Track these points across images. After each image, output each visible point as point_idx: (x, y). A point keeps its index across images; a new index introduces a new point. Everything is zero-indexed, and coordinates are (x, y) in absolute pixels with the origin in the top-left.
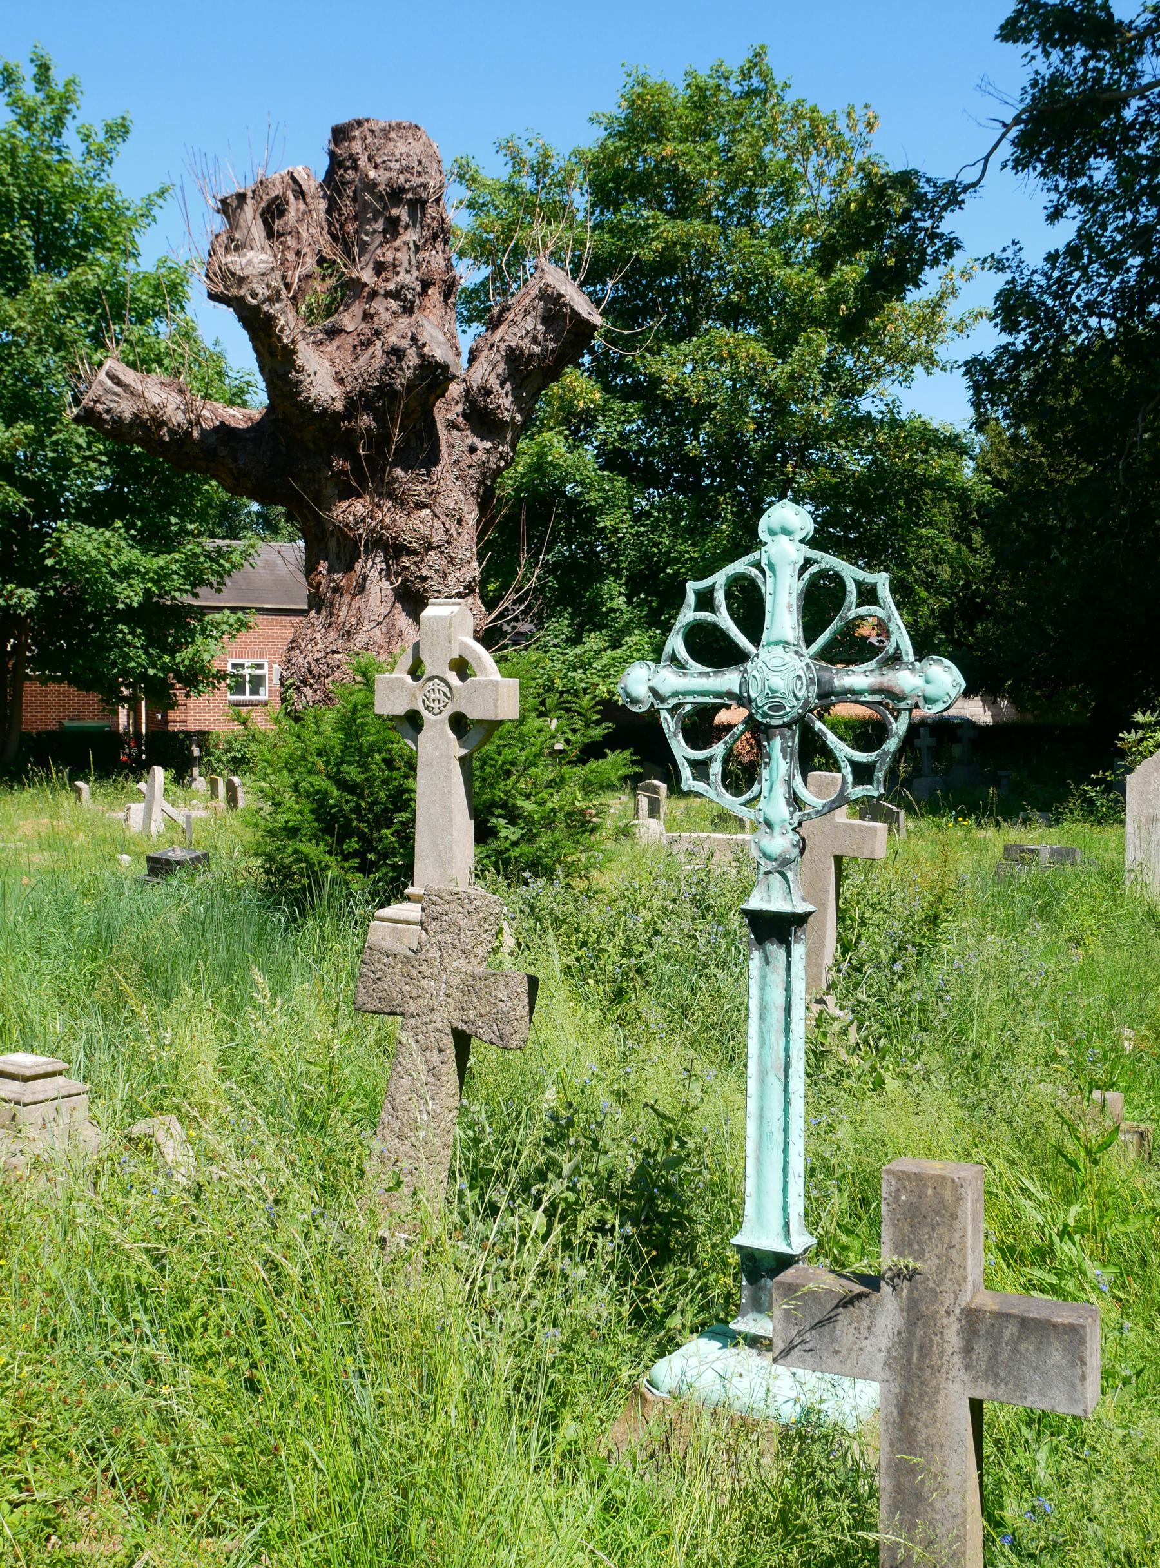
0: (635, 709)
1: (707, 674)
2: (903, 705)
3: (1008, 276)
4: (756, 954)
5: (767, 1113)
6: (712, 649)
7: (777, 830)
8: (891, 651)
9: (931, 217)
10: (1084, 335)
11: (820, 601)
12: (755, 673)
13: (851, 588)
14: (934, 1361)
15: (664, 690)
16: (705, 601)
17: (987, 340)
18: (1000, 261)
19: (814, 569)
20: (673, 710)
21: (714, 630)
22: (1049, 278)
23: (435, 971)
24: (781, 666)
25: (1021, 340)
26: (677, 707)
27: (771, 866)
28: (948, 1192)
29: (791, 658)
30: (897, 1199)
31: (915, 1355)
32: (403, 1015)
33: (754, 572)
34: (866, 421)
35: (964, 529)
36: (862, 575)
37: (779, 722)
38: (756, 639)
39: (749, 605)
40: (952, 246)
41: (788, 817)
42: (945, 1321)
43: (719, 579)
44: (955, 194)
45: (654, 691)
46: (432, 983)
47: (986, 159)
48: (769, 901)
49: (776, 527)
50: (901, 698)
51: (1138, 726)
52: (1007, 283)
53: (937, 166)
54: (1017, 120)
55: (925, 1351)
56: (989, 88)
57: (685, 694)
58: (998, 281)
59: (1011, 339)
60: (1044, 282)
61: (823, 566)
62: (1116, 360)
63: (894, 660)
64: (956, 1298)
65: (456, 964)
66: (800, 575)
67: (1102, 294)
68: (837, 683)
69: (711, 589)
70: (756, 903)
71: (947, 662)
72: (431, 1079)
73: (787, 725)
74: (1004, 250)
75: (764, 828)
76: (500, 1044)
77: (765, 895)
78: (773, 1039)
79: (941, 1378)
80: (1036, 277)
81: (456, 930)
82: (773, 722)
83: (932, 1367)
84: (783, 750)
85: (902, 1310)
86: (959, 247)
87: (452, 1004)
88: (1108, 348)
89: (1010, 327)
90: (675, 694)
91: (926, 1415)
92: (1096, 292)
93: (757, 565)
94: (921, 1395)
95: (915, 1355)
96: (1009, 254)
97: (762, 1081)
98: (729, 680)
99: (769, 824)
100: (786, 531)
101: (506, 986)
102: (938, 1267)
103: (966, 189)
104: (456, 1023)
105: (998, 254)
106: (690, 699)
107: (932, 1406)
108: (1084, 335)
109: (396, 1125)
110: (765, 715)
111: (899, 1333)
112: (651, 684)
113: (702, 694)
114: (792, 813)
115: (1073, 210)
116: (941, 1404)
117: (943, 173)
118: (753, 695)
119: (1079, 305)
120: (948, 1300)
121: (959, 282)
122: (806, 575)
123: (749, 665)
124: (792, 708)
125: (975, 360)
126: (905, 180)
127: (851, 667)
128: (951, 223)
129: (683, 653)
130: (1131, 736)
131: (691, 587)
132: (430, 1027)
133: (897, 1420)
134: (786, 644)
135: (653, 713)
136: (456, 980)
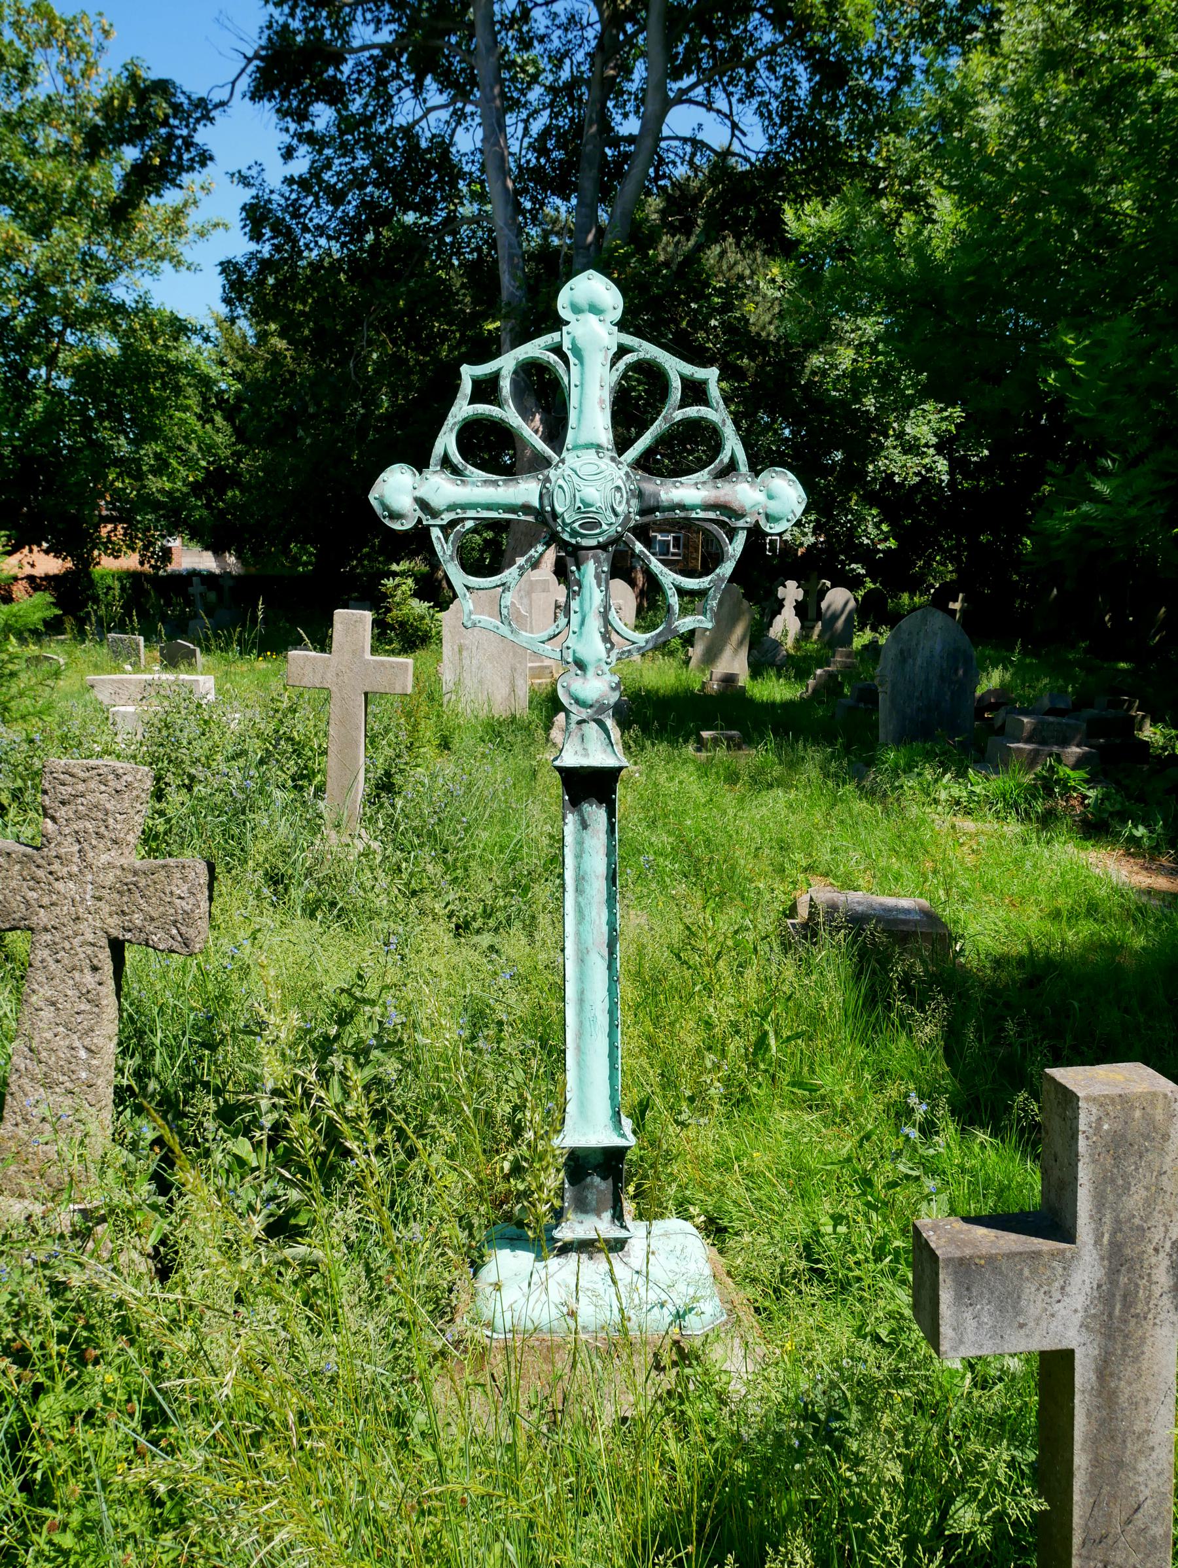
0: (396, 526)
1: (495, 483)
3: (253, 192)
4: (570, 818)
5: (588, 995)
6: (489, 448)
7: (591, 671)
8: (726, 460)
9: (187, 126)
11: (633, 404)
12: (561, 482)
13: (676, 383)
14: (1140, 1308)
15: (437, 502)
17: (238, 245)
19: (629, 358)
20: (446, 529)
22: (287, 199)
23: (75, 869)
24: (592, 477)
25: (266, 250)
26: (453, 523)
27: (585, 713)
28: (1160, 1111)
30: (1098, 1128)
31: (1118, 1307)
32: (31, 929)
33: (553, 358)
34: (120, 308)
35: (206, 411)
36: (689, 369)
37: (593, 542)
39: (545, 392)
40: (205, 158)
41: (604, 655)
42: (1153, 1260)
43: (506, 364)
45: (423, 504)
46: (71, 885)
48: (587, 755)
49: (583, 302)
50: (740, 516)
51: (395, 574)
53: (194, 82)
54: (257, 56)
55: (1128, 1300)
56: (227, 23)
57: (464, 507)
58: (246, 195)
60: (282, 202)
61: (642, 355)
62: (342, 277)
64: (1167, 1231)
65: (105, 858)
66: (613, 364)
67: (329, 220)
69: (495, 377)
70: (570, 759)
71: (791, 476)
72: (85, 1006)
73: (602, 547)
75: (574, 669)
76: (185, 951)
77: (579, 748)
78: (594, 913)
79: (1148, 1325)
81: (100, 815)
82: (585, 542)
83: (1137, 1316)
84: (597, 576)
85: (1102, 1258)
86: (211, 158)
87: (106, 908)
88: (336, 267)
89: (256, 236)
90: (451, 508)
91: (1129, 1371)
92: (325, 219)
93: (557, 350)
94: (1124, 1350)
95: (1118, 1307)
96: (254, 172)
97: (581, 961)
99: (580, 665)
100: (595, 309)
101: (184, 879)
102: (1146, 1200)
103: (216, 106)
104: (114, 933)
105: (245, 172)
106: (471, 513)
107: (1136, 1359)
108: (315, 252)
109: (39, 1071)
110: (574, 533)
111: (1099, 1286)
112: (418, 494)
113: (489, 507)
115: (303, 149)
116: (1148, 1355)
117: (199, 92)
118: (559, 509)
120: (1157, 1235)
121: (200, 195)
123: (552, 473)
124: (610, 526)
125: (229, 262)
126: (163, 87)
127: (683, 479)
128: (204, 136)
129: (456, 458)
130: (390, 583)
131: (468, 372)
132: (76, 942)
133: (1096, 1385)
134: (598, 447)
136: (110, 878)
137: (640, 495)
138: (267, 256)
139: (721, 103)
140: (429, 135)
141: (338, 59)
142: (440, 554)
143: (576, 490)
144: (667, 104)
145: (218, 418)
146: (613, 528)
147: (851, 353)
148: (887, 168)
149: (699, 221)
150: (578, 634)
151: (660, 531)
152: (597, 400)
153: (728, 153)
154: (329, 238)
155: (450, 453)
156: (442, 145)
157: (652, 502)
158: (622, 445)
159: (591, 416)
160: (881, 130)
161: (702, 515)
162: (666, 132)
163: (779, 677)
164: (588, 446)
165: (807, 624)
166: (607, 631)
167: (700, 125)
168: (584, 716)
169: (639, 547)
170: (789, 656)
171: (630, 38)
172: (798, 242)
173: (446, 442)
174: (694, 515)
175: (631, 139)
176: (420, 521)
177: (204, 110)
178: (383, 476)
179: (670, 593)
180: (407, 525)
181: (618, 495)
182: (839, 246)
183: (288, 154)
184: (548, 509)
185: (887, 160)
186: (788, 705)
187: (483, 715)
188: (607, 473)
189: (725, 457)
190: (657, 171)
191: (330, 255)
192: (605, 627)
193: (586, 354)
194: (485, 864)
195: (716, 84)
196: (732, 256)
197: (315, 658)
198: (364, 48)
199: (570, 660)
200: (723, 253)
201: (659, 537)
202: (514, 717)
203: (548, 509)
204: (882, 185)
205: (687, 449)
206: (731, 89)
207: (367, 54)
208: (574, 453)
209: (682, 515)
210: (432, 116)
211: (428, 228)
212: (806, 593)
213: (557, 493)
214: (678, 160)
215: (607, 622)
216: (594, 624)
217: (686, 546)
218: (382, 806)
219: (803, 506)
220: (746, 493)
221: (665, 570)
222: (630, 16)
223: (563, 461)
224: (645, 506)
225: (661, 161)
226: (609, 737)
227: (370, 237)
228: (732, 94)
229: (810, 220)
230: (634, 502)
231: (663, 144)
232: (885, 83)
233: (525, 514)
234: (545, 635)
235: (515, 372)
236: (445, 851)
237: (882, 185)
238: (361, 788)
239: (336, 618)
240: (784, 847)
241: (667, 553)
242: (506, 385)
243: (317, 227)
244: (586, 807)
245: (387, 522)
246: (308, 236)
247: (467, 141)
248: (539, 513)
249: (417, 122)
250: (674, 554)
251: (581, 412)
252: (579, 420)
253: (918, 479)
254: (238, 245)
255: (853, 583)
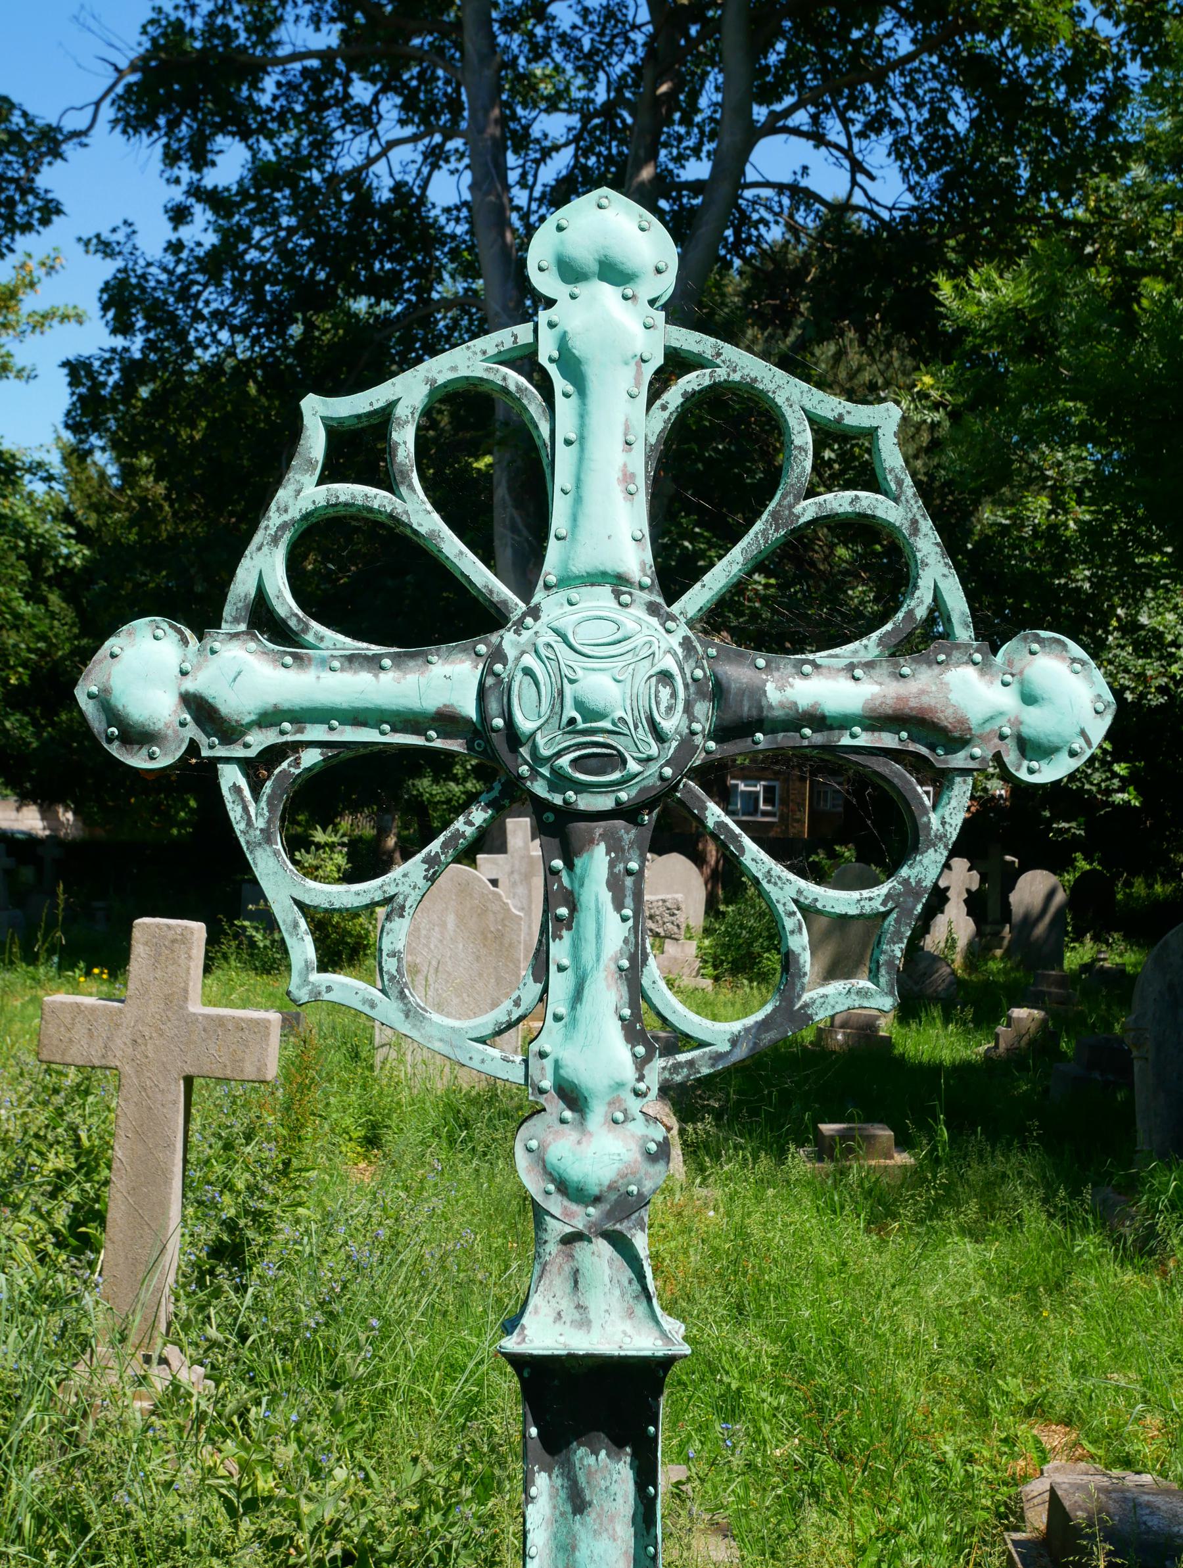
0: (138, 760)
1: (374, 663)
2: (959, 760)
3: (120, 263)
6: (376, 590)
7: (597, 1114)
8: (921, 613)
10: (213, 350)
11: (709, 469)
12: (529, 660)
13: (803, 437)
15: (236, 703)
16: (359, 451)
17: (94, 338)
18: (107, 244)
19: (692, 381)
20: (257, 769)
21: (394, 538)
22: (170, 273)
24: (602, 645)
26: (273, 755)
27: (581, 1217)
29: (637, 621)
33: (515, 379)
36: (830, 406)
37: (605, 803)
38: (525, 570)
39: (495, 466)
40: (50, 210)
41: (629, 1072)
43: (407, 392)
44: (58, 143)
45: (200, 709)
47: (97, 104)
48: (584, 1323)
49: (584, 253)
50: (956, 740)
52: (119, 271)
56: (91, 23)
58: (107, 269)
59: (127, 344)
60: (164, 277)
61: (721, 374)
62: (252, 389)
63: (924, 640)
68: (774, 694)
69: (383, 419)
70: (543, 1334)
74: (114, 230)
75: (555, 1106)
77: (566, 1305)
80: (154, 270)
82: (586, 802)
84: (614, 884)
86: (59, 212)
88: (244, 370)
89: (122, 327)
90: (269, 718)
92: (227, 301)
93: (525, 360)
96: (120, 236)
98: (446, 680)
99: (573, 1097)
100: (614, 273)
105: (106, 235)
108: (213, 350)
110: (559, 781)
112: (190, 685)
113: (357, 718)
114: (641, 1063)
117: (46, 113)
118: (525, 724)
119: (206, 311)
122: (674, 397)
123: (508, 640)
124: (645, 765)
127: (820, 657)
128: (50, 178)
129: (285, 603)
131: (316, 410)
134: (619, 582)
135: (197, 774)
137: (718, 692)
138: (138, 355)
139: (833, 128)
140: (391, 183)
141: (254, 72)
142: (239, 827)
143: (564, 679)
144: (753, 134)
145: (54, 598)
146: (653, 768)
147: (1044, 501)
148: (1099, 225)
149: (803, 307)
150: (569, 1022)
151: (744, 778)
152: (616, 474)
153: (843, 208)
154: (233, 330)
155: (271, 591)
156: (408, 200)
157: (746, 709)
158: (674, 575)
159: (604, 507)
160: (1086, 169)
161: (864, 739)
162: (751, 175)
163: (947, 1020)
164: (595, 578)
165: (988, 929)
166: (637, 1015)
167: (805, 169)
168: (580, 1224)
169: (714, 813)
170: (958, 982)
171: (692, 43)
172: (964, 330)
173: (264, 568)
174: (846, 740)
175: (697, 187)
176: (193, 748)
177: (52, 142)
178: (112, 644)
179: (789, 923)
180: (164, 759)
181: (665, 692)
182: (1026, 332)
183: (179, 215)
184: (499, 722)
185: (1097, 211)
186: (963, 1069)
187: (440, 1087)
188: (638, 640)
189: (919, 604)
190: (737, 234)
191: (234, 354)
192: (633, 1005)
193: (592, 372)
194: (417, 1405)
195: (827, 109)
196: (855, 357)
197: (93, 1009)
198: (295, 57)
199: (547, 1084)
200: (840, 355)
201: (742, 787)
202: (493, 1088)
203: (499, 722)
204: (1089, 249)
205: (824, 591)
206: (851, 114)
207: (297, 66)
208: (561, 596)
209: (819, 738)
210: (397, 154)
211: (386, 322)
212: (983, 879)
213: (521, 688)
214: (769, 217)
215: (637, 993)
216: (606, 999)
217: (784, 802)
218: (217, 1293)
219: (1108, 720)
220: (969, 690)
221: (778, 869)
222: (695, 13)
223: (535, 613)
224: (729, 717)
225: (744, 218)
226: (641, 1278)
227: (296, 330)
228: (852, 121)
229: (981, 295)
230: (703, 708)
231: (749, 194)
232: (1088, 105)
233: (443, 735)
234: (486, 1022)
235: (427, 412)
236: (335, 1386)
237: (1089, 249)
238: (175, 1257)
239: (136, 933)
240: (985, 1362)
241: (755, 810)
242: (405, 439)
243: (215, 314)
244: (581, 1455)
245: (115, 750)
246: (202, 327)
247: (448, 189)
248: (476, 732)
249: (371, 161)
250: (765, 813)
251: (578, 500)
252: (574, 519)
253: (1162, 700)
254: (94, 338)
255: (1056, 862)
